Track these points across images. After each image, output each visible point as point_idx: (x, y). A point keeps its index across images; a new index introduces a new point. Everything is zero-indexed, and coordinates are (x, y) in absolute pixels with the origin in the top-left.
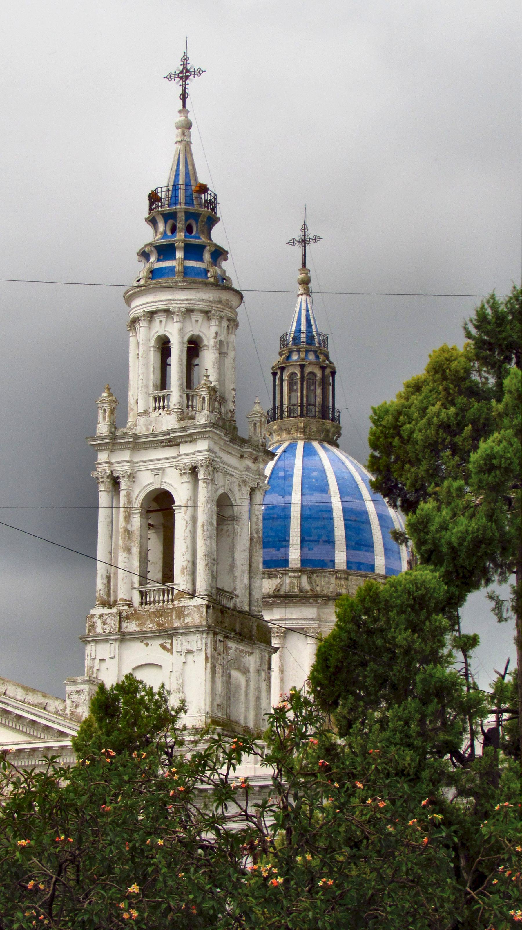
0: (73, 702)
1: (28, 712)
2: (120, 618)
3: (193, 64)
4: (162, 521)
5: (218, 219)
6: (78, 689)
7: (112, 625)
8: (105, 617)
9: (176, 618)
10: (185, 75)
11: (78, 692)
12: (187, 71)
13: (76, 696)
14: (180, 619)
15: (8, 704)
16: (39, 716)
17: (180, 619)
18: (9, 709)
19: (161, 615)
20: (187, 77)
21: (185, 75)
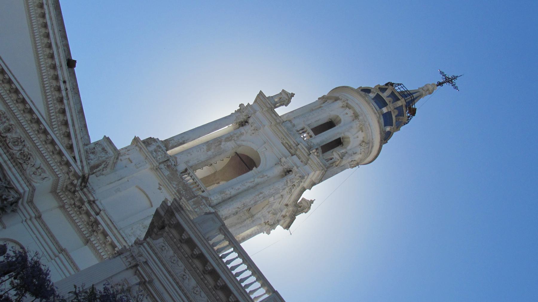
0: (94, 148)
1: (72, 116)
2: (165, 161)
3: (457, 82)
4: (218, 170)
5: (75, 61)
6: (106, 148)
7: (159, 157)
8: (160, 150)
9: (193, 202)
10: (449, 80)
11: (104, 149)
12: (451, 80)
13: (100, 149)
14: (194, 204)
15: (68, 99)
16: (73, 125)
17: (194, 204)
18: (65, 101)
19: (186, 190)
20: (448, 82)
21: (449, 80)
